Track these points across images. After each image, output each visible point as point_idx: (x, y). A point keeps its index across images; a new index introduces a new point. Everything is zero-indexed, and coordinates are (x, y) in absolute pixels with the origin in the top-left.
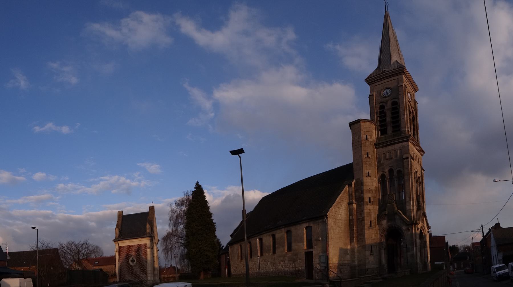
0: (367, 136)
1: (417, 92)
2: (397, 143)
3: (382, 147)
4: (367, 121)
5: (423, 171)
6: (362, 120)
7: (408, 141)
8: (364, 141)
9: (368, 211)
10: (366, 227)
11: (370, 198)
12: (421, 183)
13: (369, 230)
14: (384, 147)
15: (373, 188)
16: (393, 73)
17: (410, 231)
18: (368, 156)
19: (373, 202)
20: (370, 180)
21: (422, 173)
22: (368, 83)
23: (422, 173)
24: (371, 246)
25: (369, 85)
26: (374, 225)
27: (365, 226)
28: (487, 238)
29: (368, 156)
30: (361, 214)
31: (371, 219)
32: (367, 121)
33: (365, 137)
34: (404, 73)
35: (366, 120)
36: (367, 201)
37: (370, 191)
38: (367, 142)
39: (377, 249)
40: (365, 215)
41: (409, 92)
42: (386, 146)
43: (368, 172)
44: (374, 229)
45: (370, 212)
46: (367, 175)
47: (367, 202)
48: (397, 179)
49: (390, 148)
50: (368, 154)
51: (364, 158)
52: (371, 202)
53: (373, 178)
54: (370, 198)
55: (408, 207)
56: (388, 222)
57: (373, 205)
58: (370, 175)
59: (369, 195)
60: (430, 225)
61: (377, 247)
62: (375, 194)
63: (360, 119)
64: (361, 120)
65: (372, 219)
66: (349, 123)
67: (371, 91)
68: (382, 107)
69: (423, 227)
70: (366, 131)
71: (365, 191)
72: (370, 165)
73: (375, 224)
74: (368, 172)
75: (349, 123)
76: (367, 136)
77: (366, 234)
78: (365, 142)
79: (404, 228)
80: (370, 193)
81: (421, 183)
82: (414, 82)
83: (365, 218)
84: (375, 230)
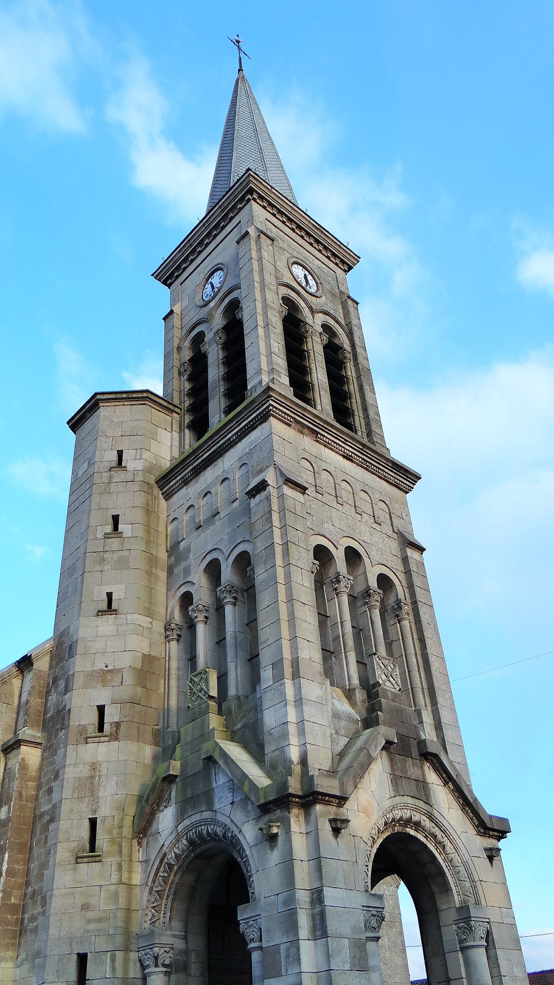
0: (120, 453)
1: (350, 268)
2: (231, 444)
3: (186, 482)
4: (124, 396)
5: (410, 552)
6: (106, 396)
7: (264, 418)
8: (106, 475)
9: (85, 771)
10: (63, 853)
11: (101, 709)
12: (407, 608)
13: (75, 870)
14: (189, 482)
15: (126, 661)
16: (223, 211)
17: (280, 840)
18: (116, 528)
19: (117, 725)
20: (110, 628)
21: (405, 560)
22: (164, 283)
23: (405, 560)
24: (82, 959)
25: (169, 286)
26: (112, 841)
27: (60, 847)
28: (360, 633)
29: (116, 528)
30: (50, 791)
31: (95, 811)
32: (124, 396)
33: (114, 456)
34: (255, 196)
35: (119, 396)
36: (84, 722)
37: (104, 676)
38: (119, 476)
39: (113, 969)
40: (67, 793)
41: (294, 263)
42: (197, 472)
43: (109, 595)
44: (107, 860)
45: (92, 777)
46: (104, 606)
47: (82, 729)
48: (235, 598)
49: (209, 475)
50: (116, 519)
51: (96, 539)
52: (107, 727)
53: (130, 617)
54: (101, 709)
55: (270, 719)
56: (181, 815)
57: (117, 739)
58: (114, 606)
59: (102, 696)
60: (491, 807)
61: (113, 960)
62: (139, 689)
63: (96, 394)
64: (98, 397)
65: (105, 811)
66: (68, 423)
67: (173, 301)
68: (199, 339)
69: (427, 823)
70: (120, 434)
71: (78, 682)
72: (122, 564)
73: (115, 832)
74: (109, 595)
75: (68, 423)
76: (120, 453)
77: (55, 892)
78: (111, 477)
79: (248, 833)
80: (104, 683)
81: (407, 608)
82: (321, 228)
83: (65, 808)
84: (114, 867)
